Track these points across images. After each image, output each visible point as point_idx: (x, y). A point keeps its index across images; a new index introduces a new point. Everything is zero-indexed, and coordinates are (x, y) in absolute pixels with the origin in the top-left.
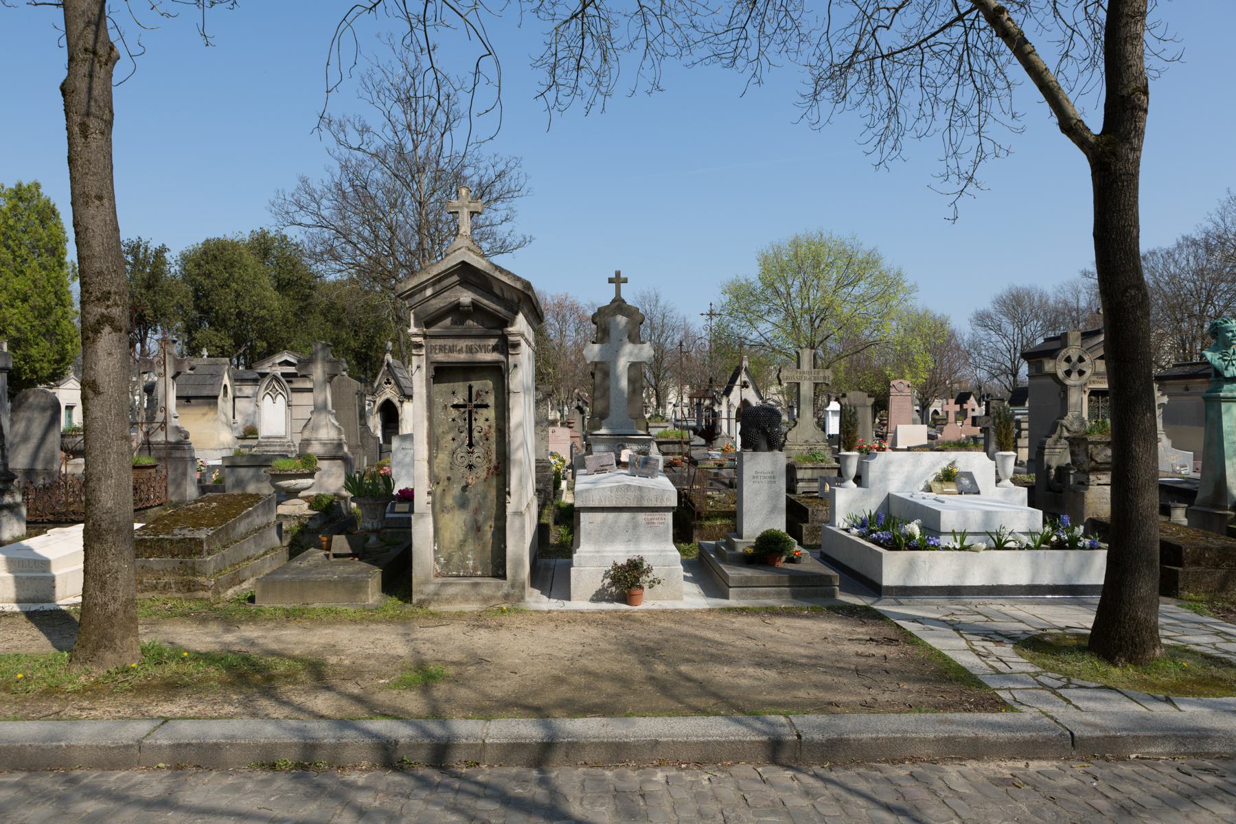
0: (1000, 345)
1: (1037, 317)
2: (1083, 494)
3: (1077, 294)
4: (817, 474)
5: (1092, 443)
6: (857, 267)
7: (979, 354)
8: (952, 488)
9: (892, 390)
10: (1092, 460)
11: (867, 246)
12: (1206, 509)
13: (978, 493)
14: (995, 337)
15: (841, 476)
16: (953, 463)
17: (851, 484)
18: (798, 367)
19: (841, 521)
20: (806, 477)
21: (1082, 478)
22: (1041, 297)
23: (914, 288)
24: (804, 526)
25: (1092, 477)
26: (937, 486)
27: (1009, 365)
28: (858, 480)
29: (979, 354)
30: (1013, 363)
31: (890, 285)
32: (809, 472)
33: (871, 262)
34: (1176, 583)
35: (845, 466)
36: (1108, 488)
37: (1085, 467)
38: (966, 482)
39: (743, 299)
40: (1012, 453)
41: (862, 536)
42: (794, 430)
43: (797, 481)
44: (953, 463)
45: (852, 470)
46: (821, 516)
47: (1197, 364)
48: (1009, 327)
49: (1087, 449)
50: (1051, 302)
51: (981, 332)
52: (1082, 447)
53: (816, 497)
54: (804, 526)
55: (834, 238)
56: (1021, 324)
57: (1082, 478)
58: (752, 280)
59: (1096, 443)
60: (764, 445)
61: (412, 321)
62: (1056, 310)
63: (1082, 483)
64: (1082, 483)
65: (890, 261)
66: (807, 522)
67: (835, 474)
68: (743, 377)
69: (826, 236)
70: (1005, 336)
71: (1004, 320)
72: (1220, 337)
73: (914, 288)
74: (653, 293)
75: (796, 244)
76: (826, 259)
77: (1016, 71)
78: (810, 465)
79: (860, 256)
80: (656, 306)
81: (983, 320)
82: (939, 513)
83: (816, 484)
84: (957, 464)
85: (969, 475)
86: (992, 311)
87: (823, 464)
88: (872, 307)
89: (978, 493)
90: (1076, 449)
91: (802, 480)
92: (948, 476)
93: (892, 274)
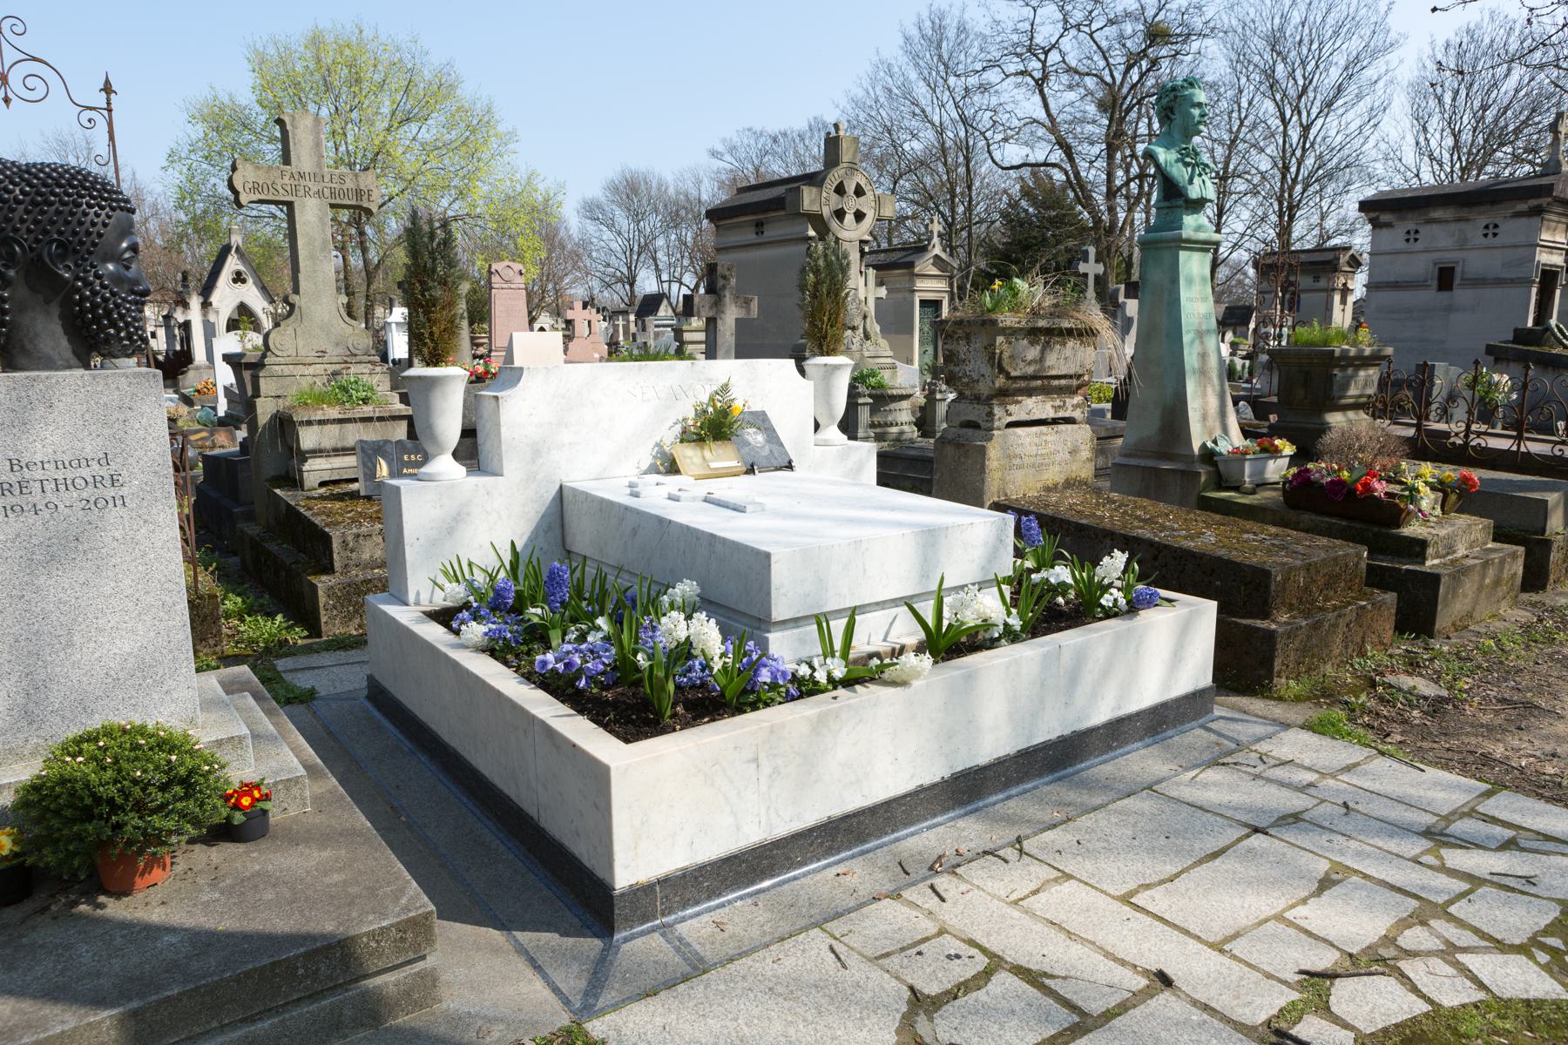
0: (614, 245)
1: (656, 211)
3: (699, 182)
4: (354, 434)
5: (1004, 331)
6: (421, 97)
8: (722, 456)
9: (495, 279)
10: (1002, 370)
11: (436, 59)
12: (1143, 463)
13: (790, 467)
14: (607, 235)
15: (415, 445)
16: (725, 388)
17: (445, 466)
18: (286, 160)
19: (426, 585)
20: (327, 444)
21: (974, 412)
22: (660, 186)
23: (512, 136)
24: (323, 583)
26: (688, 456)
27: (625, 270)
28: (471, 449)
29: (590, 256)
30: (629, 268)
31: (474, 135)
32: (334, 429)
33: (443, 89)
34: (1268, 662)
35: (427, 409)
37: (984, 388)
38: (755, 437)
41: (495, 650)
42: (288, 328)
43: (303, 456)
44: (725, 388)
45: (449, 426)
46: (371, 550)
47: (885, 251)
48: (623, 221)
49: (993, 344)
50: (671, 191)
51: (591, 227)
52: (978, 343)
53: (354, 496)
54: (323, 583)
55: (383, 38)
56: (637, 217)
57: (974, 412)
58: (244, 102)
59: (1010, 333)
60: (50, 332)
61: (1259, 623)
62: (676, 203)
63: (974, 425)
64: (974, 425)
65: (473, 88)
66: (329, 569)
67: (400, 432)
68: (232, 264)
69: (368, 34)
70: (619, 234)
71: (618, 212)
72: (1177, 117)
73: (512, 136)
75: (316, 41)
76: (372, 76)
78: (334, 413)
79: (427, 75)
81: (592, 211)
82: (768, 556)
83: (351, 461)
85: (761, 421)
86: (603, 199)
87: (367, 410)
88: (452, 161)
89: (790, 467)
90: (962, 348)
91: (317, 452)
92: (716, 426)
93: (479, 107)
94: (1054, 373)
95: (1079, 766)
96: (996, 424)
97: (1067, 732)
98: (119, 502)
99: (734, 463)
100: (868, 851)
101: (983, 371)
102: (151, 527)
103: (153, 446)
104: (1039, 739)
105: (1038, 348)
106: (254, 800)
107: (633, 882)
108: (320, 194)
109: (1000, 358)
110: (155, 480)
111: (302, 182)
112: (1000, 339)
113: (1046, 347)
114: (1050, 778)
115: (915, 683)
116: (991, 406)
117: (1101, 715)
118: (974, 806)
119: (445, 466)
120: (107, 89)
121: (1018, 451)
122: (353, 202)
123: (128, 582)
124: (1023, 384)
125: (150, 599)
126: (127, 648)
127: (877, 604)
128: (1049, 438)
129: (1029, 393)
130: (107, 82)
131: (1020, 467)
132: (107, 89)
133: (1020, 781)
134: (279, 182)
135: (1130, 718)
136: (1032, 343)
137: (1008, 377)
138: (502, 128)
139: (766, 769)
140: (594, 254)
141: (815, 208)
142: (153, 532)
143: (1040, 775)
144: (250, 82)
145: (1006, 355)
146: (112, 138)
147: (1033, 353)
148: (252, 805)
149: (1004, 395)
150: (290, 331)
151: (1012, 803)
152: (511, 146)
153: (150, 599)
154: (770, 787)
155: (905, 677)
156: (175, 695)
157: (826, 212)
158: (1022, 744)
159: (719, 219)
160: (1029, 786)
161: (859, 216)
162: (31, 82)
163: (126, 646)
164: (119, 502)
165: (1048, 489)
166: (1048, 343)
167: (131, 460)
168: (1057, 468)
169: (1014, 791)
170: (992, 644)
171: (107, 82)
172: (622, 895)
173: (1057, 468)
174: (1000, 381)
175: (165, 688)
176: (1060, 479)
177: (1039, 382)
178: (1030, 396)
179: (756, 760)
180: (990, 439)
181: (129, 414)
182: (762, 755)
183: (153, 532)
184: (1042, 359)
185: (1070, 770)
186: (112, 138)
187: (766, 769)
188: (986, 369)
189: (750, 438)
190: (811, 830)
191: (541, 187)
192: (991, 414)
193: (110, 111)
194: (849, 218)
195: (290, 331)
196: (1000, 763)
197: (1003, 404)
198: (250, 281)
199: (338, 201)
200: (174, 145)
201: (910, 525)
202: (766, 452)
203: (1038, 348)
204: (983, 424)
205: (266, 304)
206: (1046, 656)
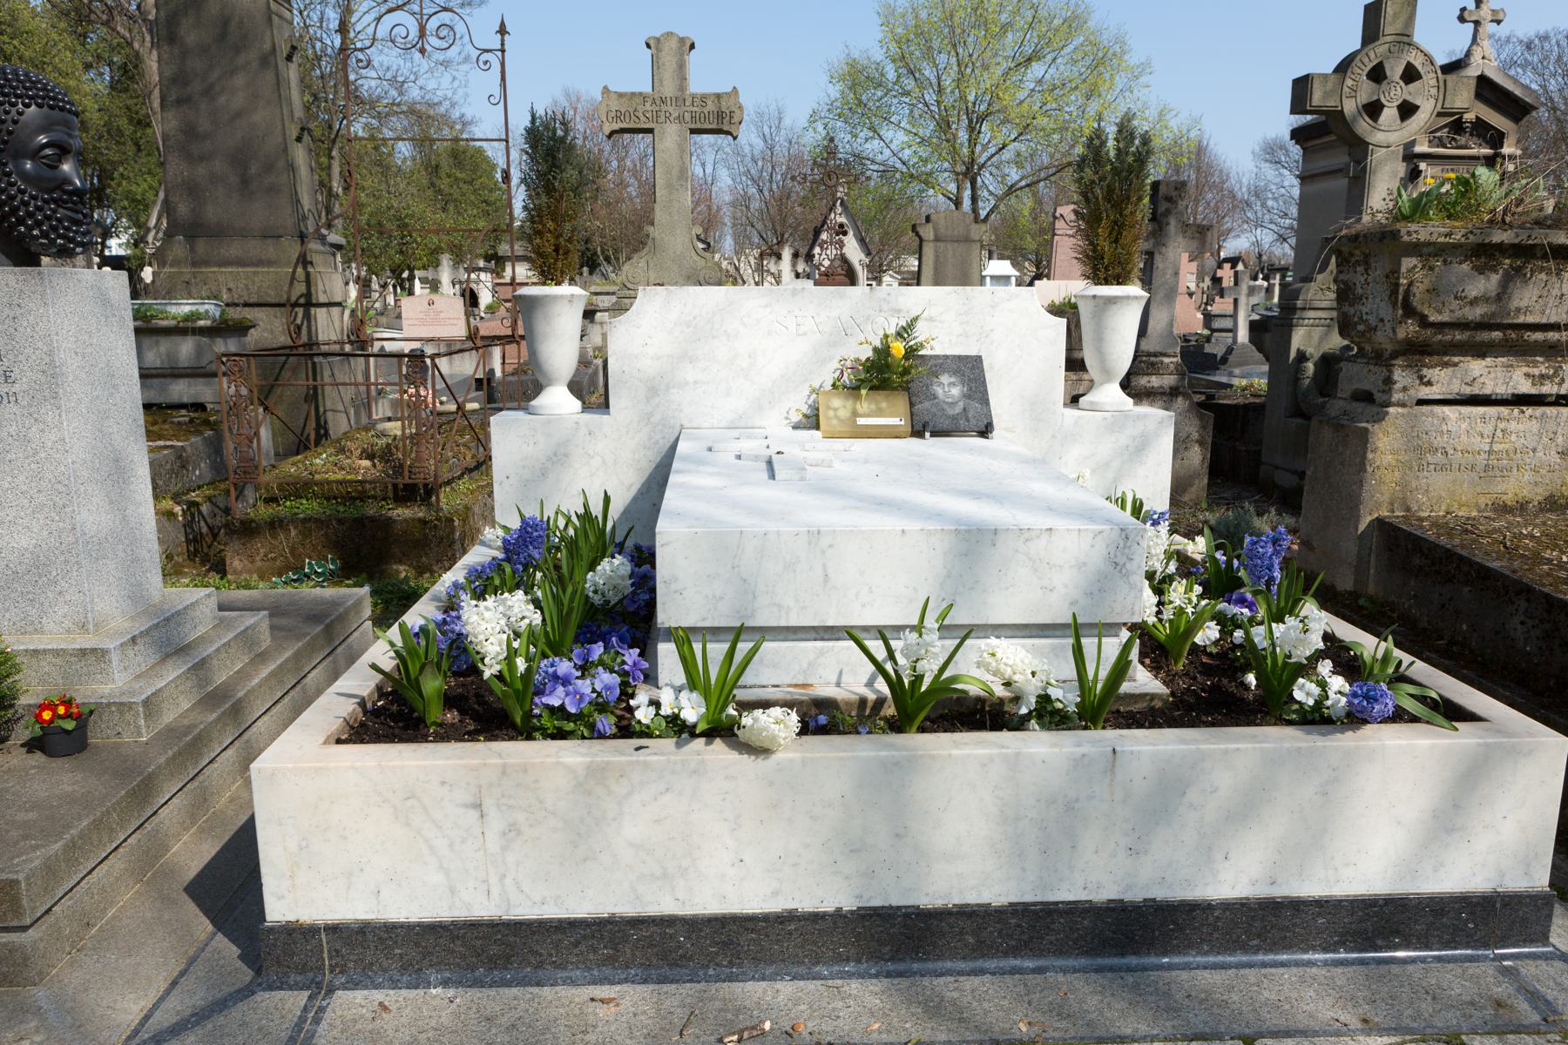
2: (1364, 436)
5: (1416, 249)
7: (1264, 205)
10: (1409, 311)
17: (558, 400)
23: (1145, 67)
25: (1401, 376)
29: (1264, 205)
36: (220, 936)
37: (1382, 339)
39: (860, 91)
40: (1134, 290)
49: (1394, 272)
51: (1269, 172)
59: (1427, 251)
73: (1145, 67)
74: (773, 107)
77: (1438, 409)
80: (778, 127)
84: (921, 333)
89: (985, 431)
90: (1358, 278)
92: (888, 374)
94: (1530, 319)
95: (1152, 960)
96: (1396, 397)
97: (1136, 895)
98: (12, 399)
99: (894, 421)
100: (1129, 969)
101: (1382, 314)
102: (42, 426)
103: (40, 344)
104: (1067, 892)
105: (1495, 278)
106: (55, 716)
107: (292, 918)
108: (681, 119)
109: (1407, 292)
110: (43, 379)
111: (664, 108)
112: (1407, 263)
113: (1515, 276)
114: (1083, 961)
115: (779, 756)
116: (1389, 368)
117: (1234, 878)
118: (901, 966)
119: (558, 400)
120: (502, 31)
121: (1439, 441)
122: (714, 126)
123: (22, 478)
124: (1459, 336)
125: (42, 498)
126: (24, 543)
127: (787, 629)
128: (1513, 425)
129: (1480, 351)
130: (503, 24)
131: (1441, 468)
132: (502, 31)
133: (1014, 952)
134: (641, 108)
135: (1296, 906)
136: (1480, 270)
137: (1424, 322)
138: (1133, 59)
139: (496, 823)
140: (1270, 203)
141: (1332, 103)
142: (42, 431)
143: (1060, 952)
144: (880, 36)
145: (1419, 289)
146: (503, 78)
147: (1484, 285)
148: (51, 721)
149: (1420, 352)
150: (642, 264)
151: (970, 983)
152: (1143, 80)
153: (42, 498)
154: (504, 848)
155: (766, 745)
156: (68, 598)
157: (1349, 107)
158: (1263, 891)
159: (1306, 140)
160: (1029, 964)
161: (1407, 110)
162: (443, 32)
163: (24, 542)
164: (12, 399)
165: (1503, 509)
166: (1518, 270)
167: (21, 358)
168: (1528, 476)
169: (992, 964)
170: (1019, 724)
171: (503, 24)
172: (271, 930)
173: (1528, 476)
174: (1410, 329)
175: (58, 589)
176: (1537, 495)
177: (1497, 335)
178: (1483, 356)
179: (478, 806)
180: (1379, 418)
181: (19, 311)
182: (488, 803)
183: (42, 431)
184: (1502, 295)
185: (1133, 960)
186: (503, 78)
187: (496, 823)
188: (1385, 311)
189: (939, 391)
190: (573, 924)
191: (1173, 123)
192: (1389, 381)
193: (503, 51)
194: (1389, 114)
195: (642, 264)
196: (967, 914)
197: (1416, 368)
198: (851, 233)
199: (699, 126)
200: (816, 106)
201: (937, 515)
202: (958, 409)
203: (1495, 278)
204: (1378, 396)
205: (863, 256)
206: (1079, 763)
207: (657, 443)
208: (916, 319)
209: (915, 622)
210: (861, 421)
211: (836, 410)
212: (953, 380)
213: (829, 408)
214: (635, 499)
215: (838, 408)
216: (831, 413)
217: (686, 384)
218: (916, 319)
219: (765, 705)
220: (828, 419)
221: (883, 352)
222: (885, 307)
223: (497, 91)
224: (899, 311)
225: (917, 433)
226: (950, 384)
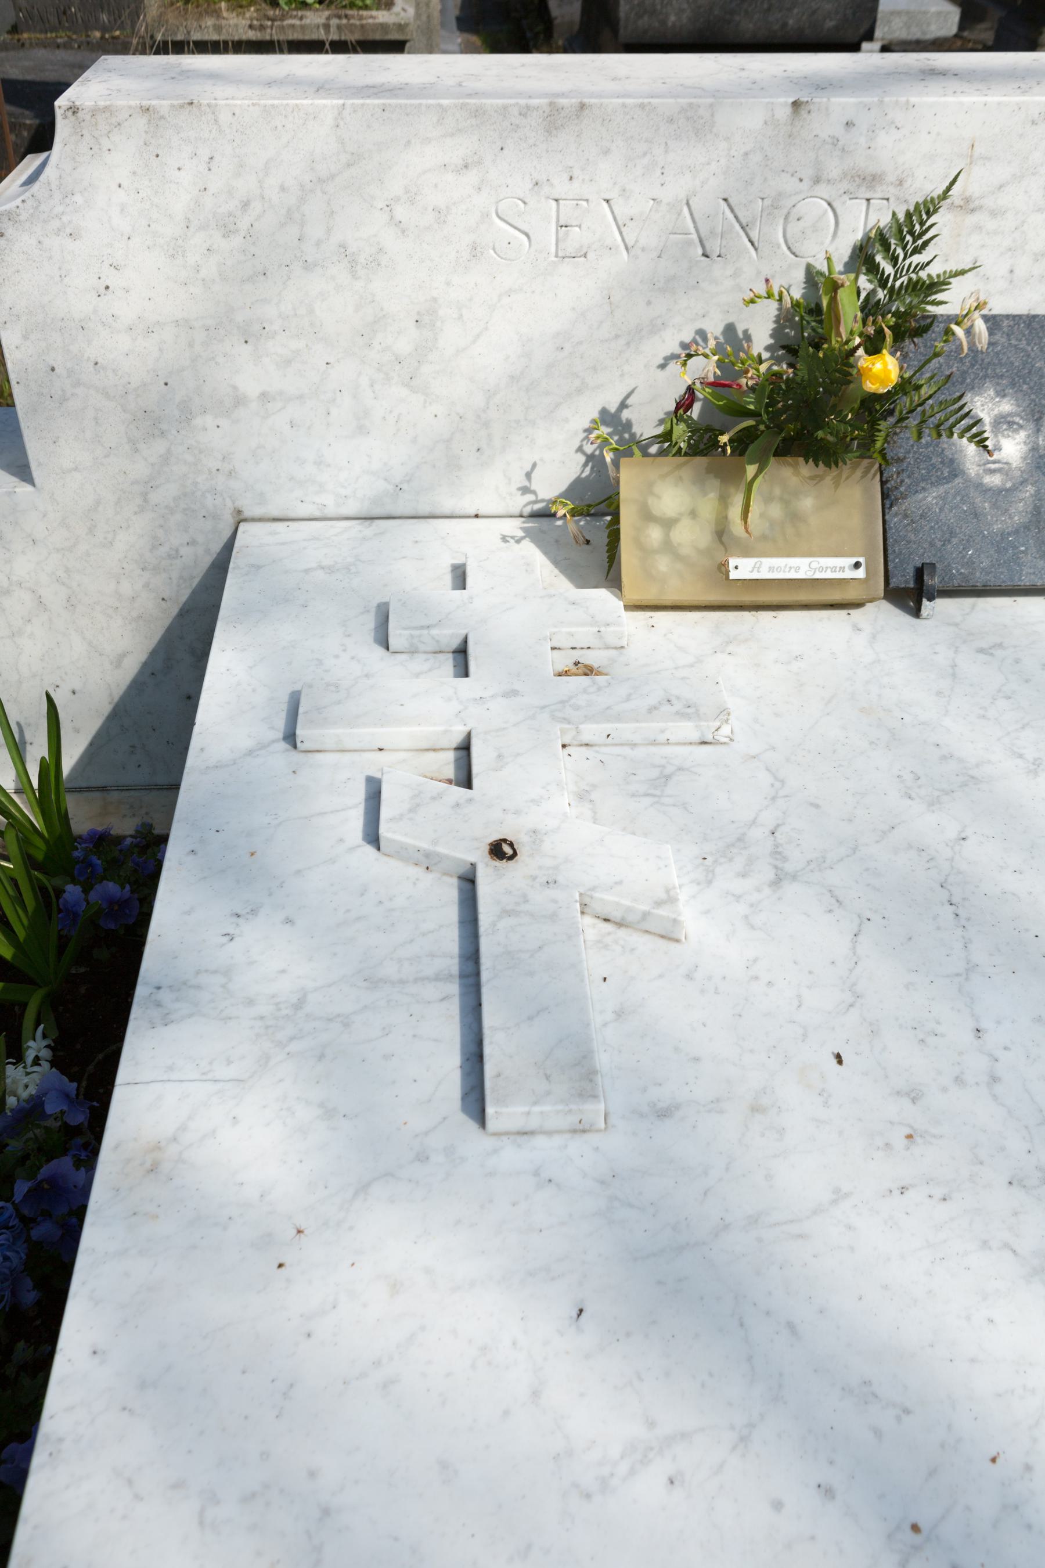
99: (835, 567)
207: (175, 554)
208: (929, 208)
209: (242, 527)
210: (744, 568)
211: (668, 524)
212: (1006, 406)
213: (648, 516)
214: (137, 686)
215: (667, 505)
216: (655, 534)
217: (239, 401)
218: (929, 208)
219: (215, 972)
220: (646, 552)
221: (807, 323)
222: (834, 168)
223: (623, 229)
224: (872, 180)
225: (911, 592)
226: (1003, 422)
